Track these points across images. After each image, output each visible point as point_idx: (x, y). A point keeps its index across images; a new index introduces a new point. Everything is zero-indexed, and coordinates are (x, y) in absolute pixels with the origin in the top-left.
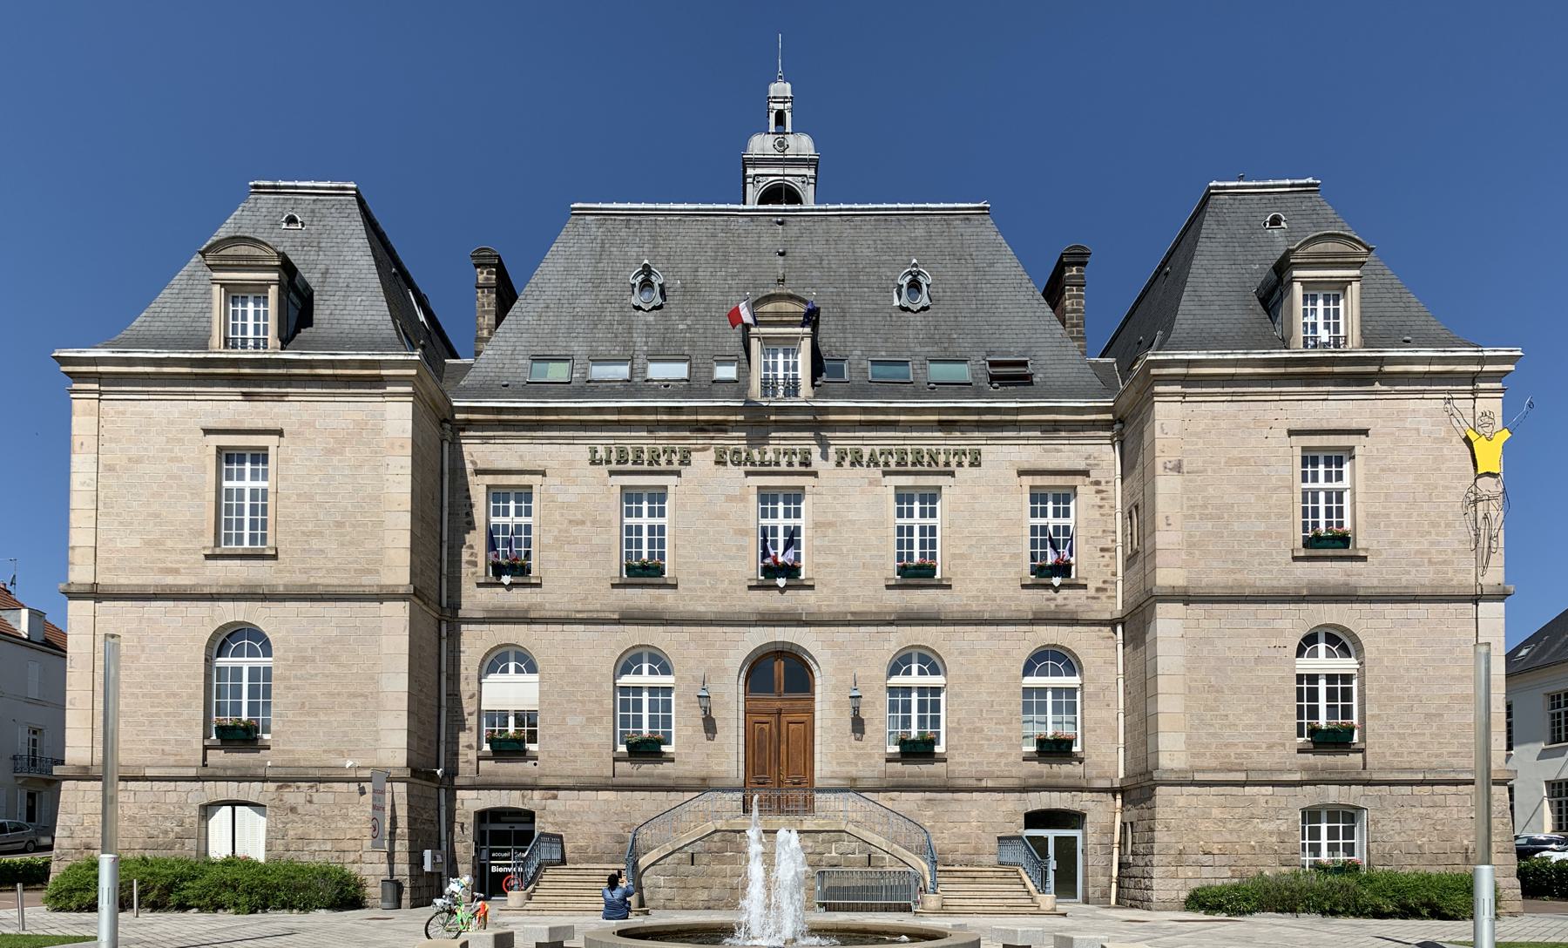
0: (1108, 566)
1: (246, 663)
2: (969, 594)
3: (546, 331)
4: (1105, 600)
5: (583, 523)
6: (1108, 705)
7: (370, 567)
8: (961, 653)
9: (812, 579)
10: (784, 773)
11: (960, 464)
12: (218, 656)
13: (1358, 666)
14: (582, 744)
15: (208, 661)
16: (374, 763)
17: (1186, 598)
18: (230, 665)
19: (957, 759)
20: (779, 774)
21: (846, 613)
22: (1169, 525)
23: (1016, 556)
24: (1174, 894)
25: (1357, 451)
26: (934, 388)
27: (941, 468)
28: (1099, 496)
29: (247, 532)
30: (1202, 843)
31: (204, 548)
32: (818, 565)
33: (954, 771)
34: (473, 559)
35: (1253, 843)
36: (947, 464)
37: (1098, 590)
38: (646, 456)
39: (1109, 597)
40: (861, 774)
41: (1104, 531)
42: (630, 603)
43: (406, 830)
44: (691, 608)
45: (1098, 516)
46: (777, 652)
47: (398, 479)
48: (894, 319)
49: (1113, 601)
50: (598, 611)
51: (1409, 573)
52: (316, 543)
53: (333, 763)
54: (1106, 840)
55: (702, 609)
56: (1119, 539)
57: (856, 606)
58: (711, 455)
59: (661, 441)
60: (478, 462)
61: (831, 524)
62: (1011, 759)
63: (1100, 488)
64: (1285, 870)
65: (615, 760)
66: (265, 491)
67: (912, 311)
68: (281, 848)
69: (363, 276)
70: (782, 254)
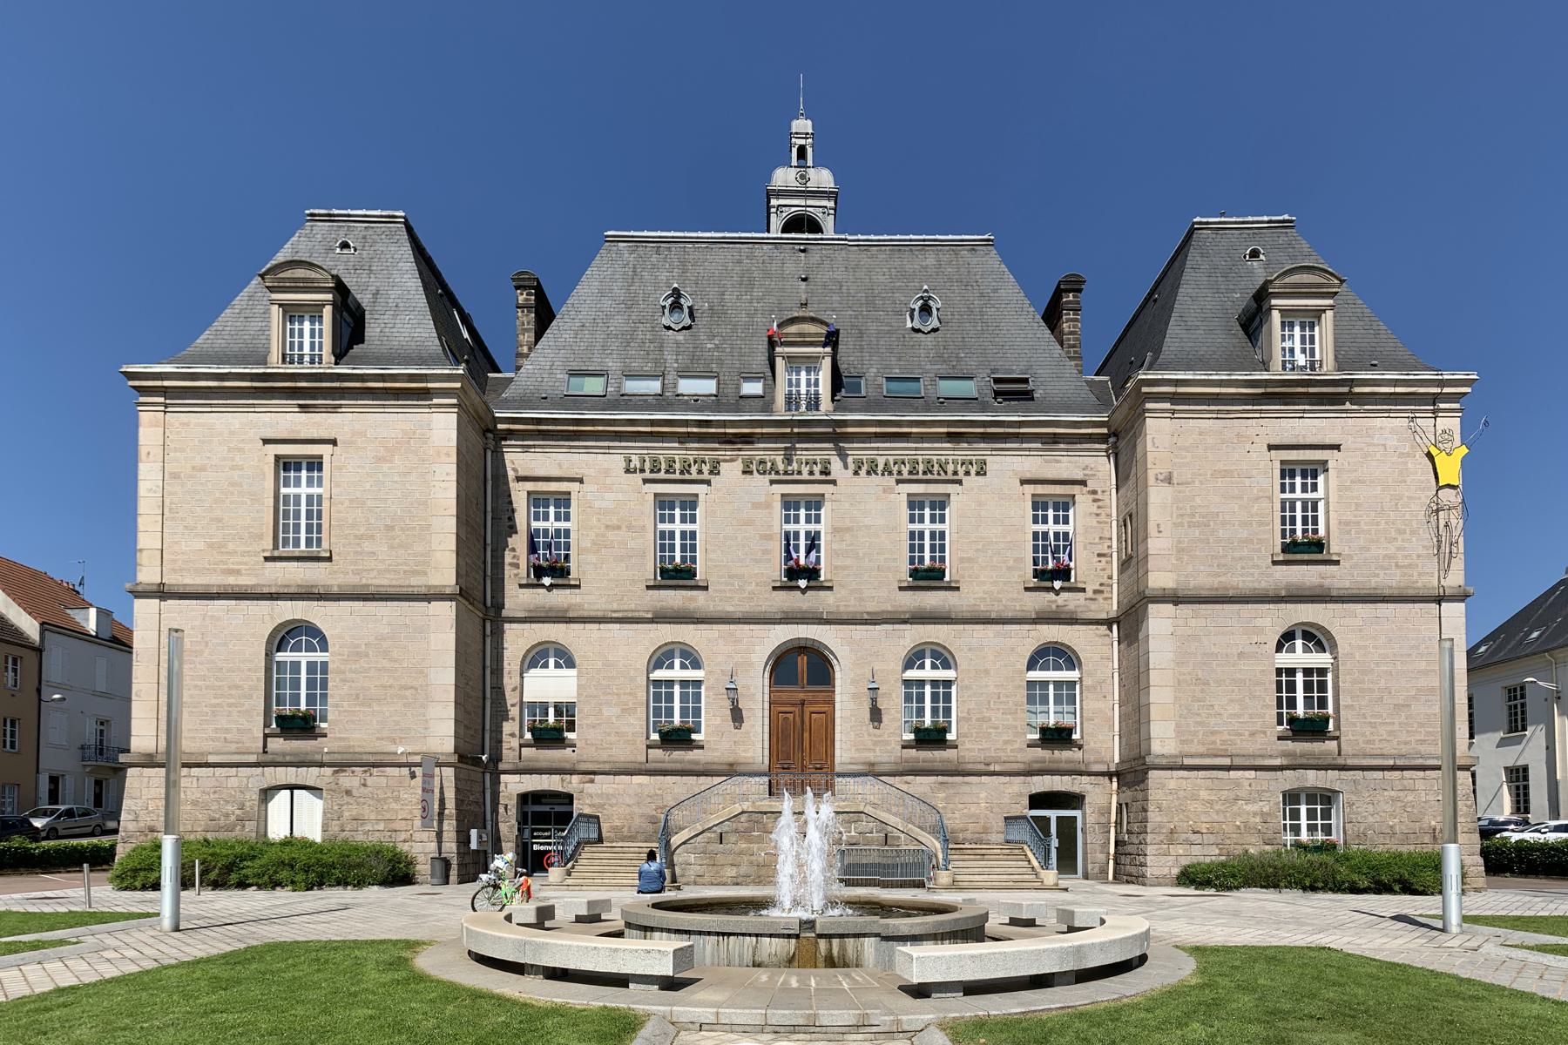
0: (1104, 570)
1: (304, 658)
4: (1102, 601)
5: (619, 528)
8: (970, 650)
10: (808, 759)
11: (967, 473)
13: (1332, 661)
15: (269, 655)
16: (424, 749)
17: (1176, 599)
19: (968, 746)
22: (1160, 532)
26: (943, 403)
28: (1096, 504)
29: (303, 535)
31: (264, 551)
34: (515, 561)
35: (1238, 823)
36: (955, 473)
37: (1095, 592)
39: (1106, 599)
41: (1101, 538)
43: (454, 811)
47: (443, 485)
49: (1109, 602)
51: (1378, 576)
55: (731, 609)
57: (872, 607)
58: (738, 466)
59: (692, 452)
61: (849, 529)
62: (1016, 746)
63: (1097, 497)
64: (1268, 848)
65: (648, 747)
66: (320, 497)
67: (924, 333)
68: (337, 828)
70: (804, 280)
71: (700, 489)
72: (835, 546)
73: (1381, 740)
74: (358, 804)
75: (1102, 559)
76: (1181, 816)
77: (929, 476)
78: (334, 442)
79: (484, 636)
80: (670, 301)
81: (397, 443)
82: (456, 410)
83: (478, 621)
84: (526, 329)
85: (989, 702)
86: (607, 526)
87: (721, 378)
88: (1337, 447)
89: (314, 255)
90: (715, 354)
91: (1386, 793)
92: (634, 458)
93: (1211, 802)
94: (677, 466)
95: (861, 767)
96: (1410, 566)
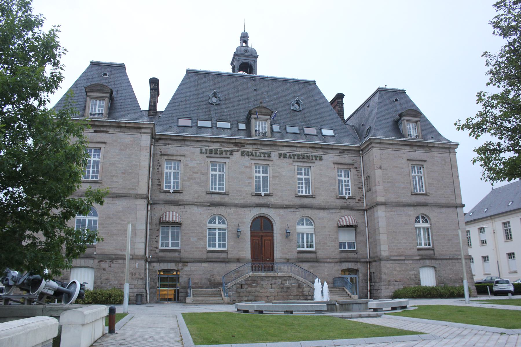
0: (361, 193)
3: (182, 109)
5: (197, 173)
6: (364, 236)
7: (133, 188)
8: (319, 219)
9: (272, 194)
10: (264, 257)
11: (316, 159)
13: (430, 226)
14: (196, 247)
17: (385, 204)
19: (320, 253)
22: (379, 184)
23: (334, 189)
25: (424, 166)
26: (306, 136)
28: (357, 172)
29: (91, 174)
30: (395, 278)
32: (274, 189)
33: (319, 257)
34: (159, 183)
35: (408, 278)
36: (312, 159)
37: (359, 200)
39: (362, 203)
42: (213, 200)
44: (233, 202)
45: (357, 178)
46: (261, 217)
47: (144, 159)
49: (363, 204)
51: (440, 200)
52: (115, 179)
53: (118, 253)
56: (364, 185)
57: (286, 203)
58: (239, 153)
59: (225, 147)
60: (162, 152)
61: (278, 177)
62: (336, 253)
64: (417, 286)
68: (99, 283)
69: (130, 93)
70: (255, 90)
71: (226, 160)
72: (273, 182)
73: (445, 250)
74: (108, 274)
75: (360, 189)
78: (105, 143)
81: (128, 145)
82: (150, 135)
83: (146, 205)
84: (153, 97)
86: (193, 172)
88: (425, 161)
89: (94, 77)
91: (448, 267)
92: (203, 149)
93: (400, 271)
94: (218, 152)
95: (284, 260)
96: (448, 197)
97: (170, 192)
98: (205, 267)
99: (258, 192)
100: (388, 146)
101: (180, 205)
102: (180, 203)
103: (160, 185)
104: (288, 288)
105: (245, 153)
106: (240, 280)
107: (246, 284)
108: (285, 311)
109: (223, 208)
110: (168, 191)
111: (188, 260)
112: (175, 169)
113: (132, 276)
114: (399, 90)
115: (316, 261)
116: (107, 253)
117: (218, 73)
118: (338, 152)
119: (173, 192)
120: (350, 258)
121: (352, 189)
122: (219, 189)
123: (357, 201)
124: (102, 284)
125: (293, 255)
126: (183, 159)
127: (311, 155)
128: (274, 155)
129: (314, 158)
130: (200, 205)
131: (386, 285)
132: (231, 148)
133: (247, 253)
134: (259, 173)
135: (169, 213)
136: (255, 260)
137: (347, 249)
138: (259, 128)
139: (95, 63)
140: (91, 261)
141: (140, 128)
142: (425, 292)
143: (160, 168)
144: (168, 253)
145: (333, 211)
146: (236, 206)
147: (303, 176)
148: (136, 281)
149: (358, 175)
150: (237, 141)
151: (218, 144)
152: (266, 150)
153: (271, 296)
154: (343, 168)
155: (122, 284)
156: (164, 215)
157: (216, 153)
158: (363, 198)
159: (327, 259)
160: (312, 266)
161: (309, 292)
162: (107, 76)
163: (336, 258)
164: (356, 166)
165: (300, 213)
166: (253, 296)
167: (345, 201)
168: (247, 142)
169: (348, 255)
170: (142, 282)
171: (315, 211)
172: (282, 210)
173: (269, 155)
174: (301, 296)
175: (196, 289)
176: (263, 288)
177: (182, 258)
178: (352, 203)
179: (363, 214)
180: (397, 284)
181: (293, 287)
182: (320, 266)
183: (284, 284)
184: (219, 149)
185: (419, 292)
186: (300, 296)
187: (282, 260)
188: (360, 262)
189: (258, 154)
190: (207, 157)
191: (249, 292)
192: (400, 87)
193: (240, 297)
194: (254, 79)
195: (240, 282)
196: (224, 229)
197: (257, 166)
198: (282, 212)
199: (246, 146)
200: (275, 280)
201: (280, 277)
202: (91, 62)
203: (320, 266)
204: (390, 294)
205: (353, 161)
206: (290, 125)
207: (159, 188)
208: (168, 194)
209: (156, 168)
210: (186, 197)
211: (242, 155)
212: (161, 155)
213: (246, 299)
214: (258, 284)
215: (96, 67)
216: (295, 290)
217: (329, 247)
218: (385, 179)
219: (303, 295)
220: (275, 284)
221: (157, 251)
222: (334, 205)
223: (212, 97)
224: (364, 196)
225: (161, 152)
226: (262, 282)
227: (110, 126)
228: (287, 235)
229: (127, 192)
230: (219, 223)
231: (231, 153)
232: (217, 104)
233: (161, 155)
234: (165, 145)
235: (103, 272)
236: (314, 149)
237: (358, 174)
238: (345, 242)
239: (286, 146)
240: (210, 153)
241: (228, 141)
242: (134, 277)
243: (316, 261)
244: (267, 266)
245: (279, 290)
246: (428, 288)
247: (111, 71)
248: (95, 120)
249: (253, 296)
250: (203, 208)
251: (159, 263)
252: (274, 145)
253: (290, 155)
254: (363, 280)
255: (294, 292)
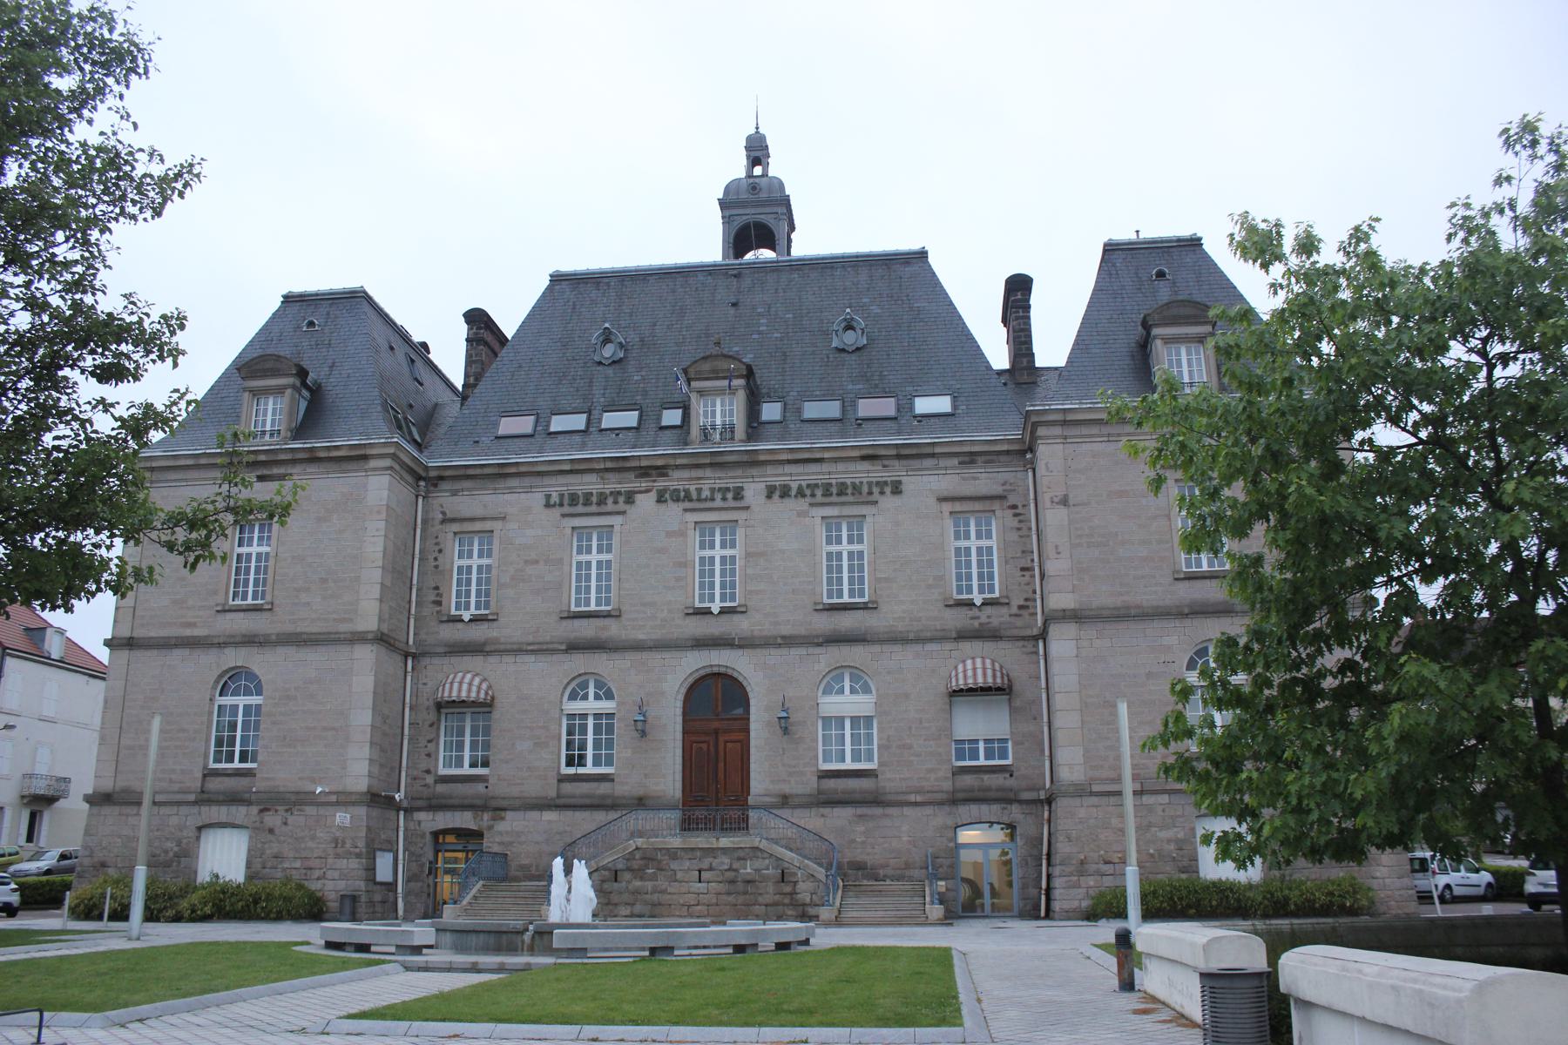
0: (1028, 584)
1: (241, 701)
2: (895, 616)
4: (1027, 617)
5: (537, 562)
7: (346, 616)
8: (889, 673)
11: (882, 493)
12: (221, 695)
14: (529, 768)
16: (340, 789)
17: (1076, 616)
18: (229, 703)
19: (888, 775)
20: (717, 792)
21: (776, 638)
22: (1059, 553)
24: (1076, 904)
26: (860, 425)
27: (865, 498)
28: (1017, 519)
29: (251, 589)
30: (1102, 852)
31: (217, 605)
34: (438, 599)
35: (1151, 851)
36: (870, 493)
37: (1021, 607)
38: (594, 499)
40: (795, 791)
41: (1023, 552)
43: (364, 850)
47: (373, 539)
48: (831, 359)
50: (547, 643)
54: (1035, 852)
55: (641, 637)
57: (786, 630)
58: (653, 495)
59: (612, 484)
61: (762, 554)
62: (941, 774)
63: (1017, 511)
64: (1184, 876)
65: (560, 781)
67: (848, 352)
68: (259, 866)
70: (734, 305)
71: (616, 521)
74: (279, 842)
76: (1092, 846)
77: (843, 499)
79: (406, 672)
80: (601, 339)
85: (910, 728)
86: (526, 562)
87: (644, 409)
90: (642, 385)
92: (554, 494)
97: (463, 621)
98: (550, 822)
99: (965, 596)
100: (1094, 430)
101: (489, 653)
102: (488, 648)
103: (439, 603)
104: (749, 882)
105: (667, 496)
106: (610, 860)
107: (629, 869)
108: (397, 946)
109: (604, 656)
110: (458, 618)
111: (504, 803)
112: (850, 541)
113: (336, 847)
114: (1179, 240)
115: (876, 800)
116: (282, 789)
117: (636, 271)
118: (955, 461)
119: (471, 620)
120: (988, 789)
121: (1000, 575)
122: (852, 593)
123: (1014, 610)
124: (264, 868)
125: (806, 784)
126: (500, 527)
127: (865, 480)
128: (754, 491)
129: (876, 490)
130: (541, 649)
131: (1071, 874)
132: (629, 483)
133: (668, 779)
134: (967, 537)
135: (974, 664)
136: (697, 801)
137: (982, 762)
138: (713, 415)
139: (293, 297)
140: (243, 810)
141: (365, 458)
142: (1181, 899)
143: (440, 557)
144: (459, 785)
145: (930, 647)
146: (638, 647)
147: (845, 547)
148: (345, 861)
149: (1019, 529)
150: (644, 463)
151: (593, 478)
152: (728, 480)
153: (697, 905)
154: (973, 511)
155: (311, 869)
156: (953, 673)
157: (587, 503)
158: (1035, 600)
159: (911, 793)
160: (860, 816)
161: (812, 894)
162: (317, 328)
163: (942, 792)
164: (1012, 500)
165: (828, 657)
166: (646, 903)
167: (975, 612)
168: (672, 462)
169: (982, 780)
170: (359, 863)
171: (876, 648)
172: (773, 651)
173: (738, 494)
174: (788, 905)
175: (524, 883)
176: (676, 881)
177: (618, 797)
178: (997, 617)
179: (1034, 650)
180: (1111, 872)
181: (765, 879)
182: (887, 816)
183: (736, 870)
184: (594, 491)
185: (1157, 898)
186: (784, 905)
187: (768, 799)
188: (1020, 802)
189: (706, 493)
190: (563, 516)
191: (637, 892)
192: (1184, 232)
193: (611, 907)
194: (735, 272)
195: (610, 865)
196: (610, 716)
197: (831, 523)
198: (774, 656)
199: (670, 472)
200: (711, 860)
201: (725, 850)
202: (284, 297)
203: (887, 816)
204: (1085, 904)
205: (1003, 485)
206: (816, 396)
207: (438, 612)
208: (460, 625)
209: (431, 558)
210: (508, 630)
211: (660, 500)
212: (443, 522)
213: (628, 912)
214: (662, 870)
215: (296, 307)
216: (771, 888)
217: (919, 755)
218: (1080, 536)
219: (794, 904)
220: (711, 869)
221: (430, 780)
222: (938, 627)
223: (841, 330)
224: (1038, 592)
225: (444, 513)
226: (674, 865)
227: (294, 462)
228: (785, 726)
229: (330, 630)
230: (597, 697)
231: (630, 498)
232: (614, 362)
233: (443, 522)
234: (454, 493)
235: (270, 837)
236: (875, 462)
237: (1022, 525)
238: (977, 741)
239: (789, 462)
240: (570, 505)
241: (619, 466)
242: (339, 850)
243: (876, 800)
244: (731, 817)
245: (722, 887)
246: (1225, 883)
247: (328, 314)
248: (256, 448)
249: (646, 903)
250: (549, 658)
251: (431, 813)
252: (752, 462)
253: (800, 488)
254: (1029, 859)
255: (767, 893)
